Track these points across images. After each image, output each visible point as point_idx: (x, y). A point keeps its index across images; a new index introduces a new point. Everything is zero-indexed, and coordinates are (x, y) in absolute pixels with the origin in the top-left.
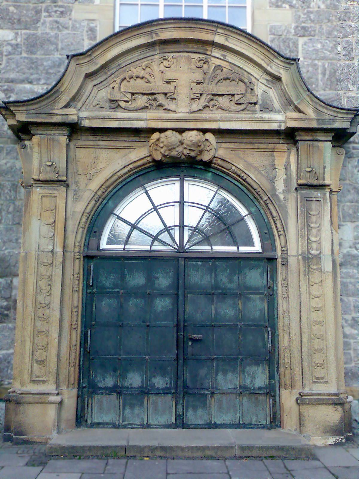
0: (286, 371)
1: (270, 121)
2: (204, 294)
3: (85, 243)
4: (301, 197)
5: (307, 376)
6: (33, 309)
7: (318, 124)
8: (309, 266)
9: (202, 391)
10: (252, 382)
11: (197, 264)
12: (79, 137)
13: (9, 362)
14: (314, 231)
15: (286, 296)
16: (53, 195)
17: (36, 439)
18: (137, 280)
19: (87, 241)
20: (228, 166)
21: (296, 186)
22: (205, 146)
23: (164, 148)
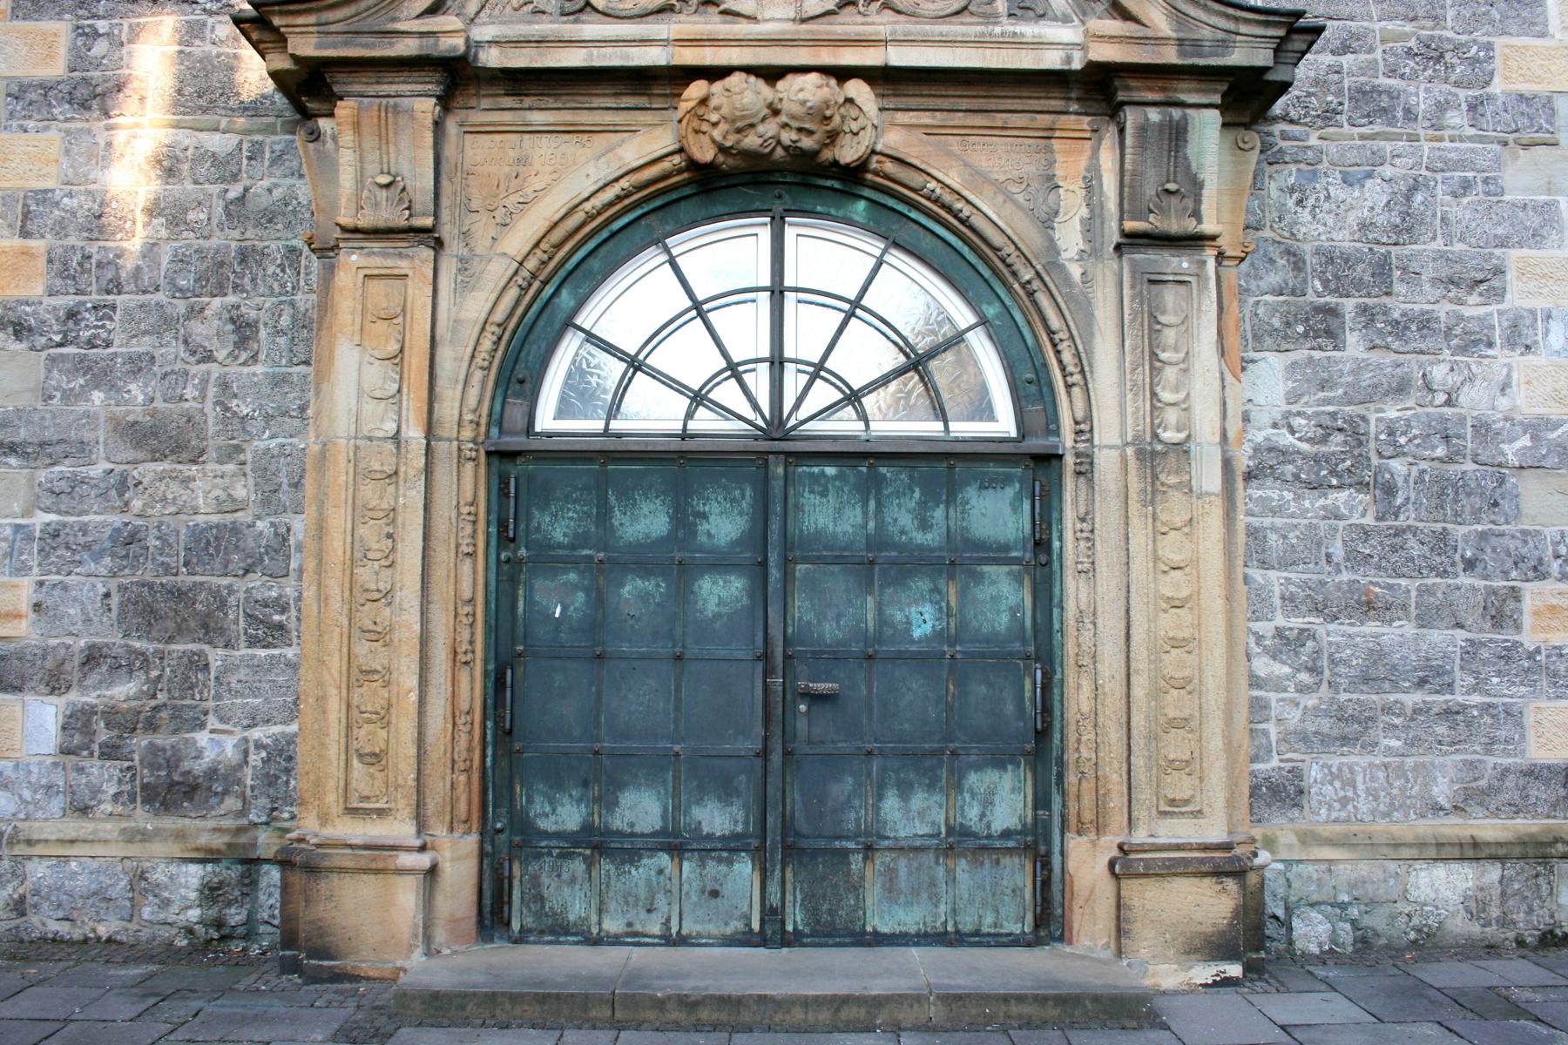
0: (1084, 784)
1: (1039, 44)
2: (839, 560)
3: (490, 415)
4: (1133, 273)
5: (1144, 795)
6: (347, 606)
7: (1182, 54)
8: (1155, 477)
9: (837, 844)
10: (983, 815)
11: (823, 474)
12: (473, 102)
13: (290, 758)
14: (1170, 374)
15: (1086, 566)
16: (396, 272)
17: (366, 968)
18: (647, 521)
19: (498, 407)
20: (916, 179)
21: (1116, 238)
22: (843, 117)
23: (723, 127)
